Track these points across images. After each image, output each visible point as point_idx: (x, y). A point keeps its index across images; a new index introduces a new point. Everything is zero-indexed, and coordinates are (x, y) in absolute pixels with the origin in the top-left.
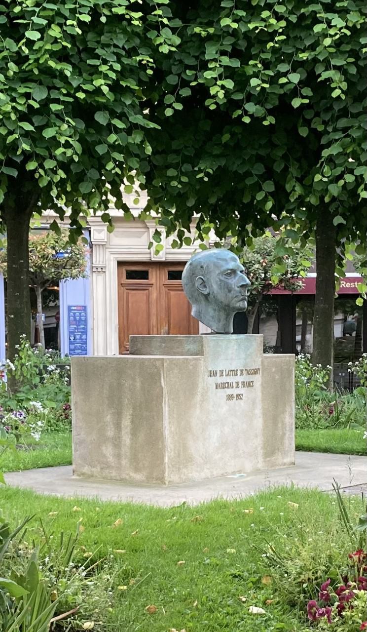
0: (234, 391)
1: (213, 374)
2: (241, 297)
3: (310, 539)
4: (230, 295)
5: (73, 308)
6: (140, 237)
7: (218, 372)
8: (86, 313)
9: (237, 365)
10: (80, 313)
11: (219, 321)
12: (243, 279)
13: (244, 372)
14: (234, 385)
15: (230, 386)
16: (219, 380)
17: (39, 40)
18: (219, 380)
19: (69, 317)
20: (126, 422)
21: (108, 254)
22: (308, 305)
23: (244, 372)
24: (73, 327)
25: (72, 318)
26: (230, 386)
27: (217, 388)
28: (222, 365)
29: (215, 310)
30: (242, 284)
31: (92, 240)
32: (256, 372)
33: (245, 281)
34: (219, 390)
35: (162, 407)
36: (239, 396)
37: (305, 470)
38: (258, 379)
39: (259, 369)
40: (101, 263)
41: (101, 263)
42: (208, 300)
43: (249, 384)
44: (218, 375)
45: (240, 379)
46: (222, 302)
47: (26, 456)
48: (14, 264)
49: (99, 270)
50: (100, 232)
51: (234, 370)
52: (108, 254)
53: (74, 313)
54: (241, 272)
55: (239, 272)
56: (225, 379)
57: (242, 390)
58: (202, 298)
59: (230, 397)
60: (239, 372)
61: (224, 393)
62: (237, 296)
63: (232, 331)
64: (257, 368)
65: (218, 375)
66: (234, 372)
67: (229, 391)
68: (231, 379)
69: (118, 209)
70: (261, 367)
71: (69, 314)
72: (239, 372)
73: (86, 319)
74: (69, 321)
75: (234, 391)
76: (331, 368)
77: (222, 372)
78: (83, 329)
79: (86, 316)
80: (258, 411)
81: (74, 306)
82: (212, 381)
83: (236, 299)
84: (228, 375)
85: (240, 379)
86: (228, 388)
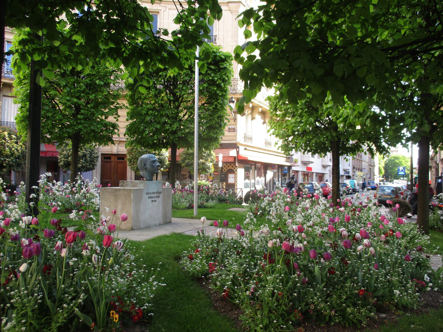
0: (154, 199)
1: (147, 194)
3: (64, 253)
9: (155, 190)
17: (358, 233)
22: (172, 246)
32: (160, 193)
36: (155, 201)
37: (205, 210)
45: (156, 195)
47: (288, 174)
57: (156, 199)
59: (152, 201)
61: (150, 200)
66: (154, 193)
67: (152, 199)
69: (145, 7)
75: (154, 199)
76: (235, 267)
80: (161, 205)
82: (147, 196)
85: (156, 195)
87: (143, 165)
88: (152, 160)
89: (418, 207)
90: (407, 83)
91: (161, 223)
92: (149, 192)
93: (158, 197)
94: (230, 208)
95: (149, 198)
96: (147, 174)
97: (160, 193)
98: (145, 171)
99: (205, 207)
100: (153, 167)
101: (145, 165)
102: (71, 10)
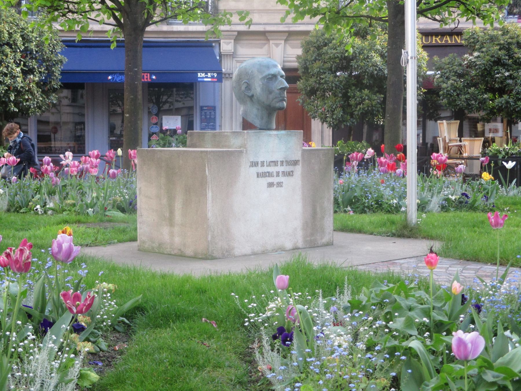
0: (275, 180)
1: (254, 164)
2: (281, 98)
4: (271, 97)
5: (205, 108)
6: (261, 48)
7: (260, 163)
8: (215, 113)
9: (278, 156)
10: (210, 113)
11: (262, 118)
12: (282, 83)
13: (284, 164)
14: (275, 174)
15: (269, 174)
16: (261, 170)
18: (261, 170)
19: (201, 116)
20: (178, 205)
21: (234, 62)
23: (284, 164)
24: (204, 124)
25: (203, 117)
26: (269, 174)
27: (258, 177)
28: (264, 156)
29: (258, 109)
30: (281, 87)
31: (221, 51)
32: (295, 163)
33: (284, 84)
34: (260, 179)
35: (206, 192)
36: (280, 184)
38: (298, 170)
39: (298, 161)
40: (228, 70)
41: (228, 70)
42: (252, 101)
43: (289, 174)
44: (260, 165)
45: (281, 169)
46: (263, 103)
48: (130, 71)
49: (227, 76)
50: (228, 44)
51: (274, 162)
52: (234, 62)
53: (205, 113)
54: (282, 76)
55: (279, 77)
56: (266, 169)
58: (248, 99)
59: (271, 185)
60: (279, 163)
62: (276, 98)
63: (274, 127)
64: (297, 159)
65: (260, 165)
67: (270, 180)
68: (273, 169)
70: (300, 159)
71: (201, 113)
72: (279, 163)
73: (215, 117)
74: (201, 119)
77: (263, 163)
78: (213, 126)
79: (215, 115)
81: (206, 107)
82: (254, 170)
83: (276, 100)
84: (269, 165)
85: (281, 169)
86: (269, 176)
87: (243, 88)
88: (267, 73)
89: (112, 224)
90: (397, 334)
91: (300, 244)
92: (260, 160)
93: (290, 174)
94: (208, 168)
95: (258, 175)
96: (255, 111)
97: (295, 163)
98: (249, 103)
99: (473, 208)
100: (270, 92)
101: (249, 87)
102: (515, 181)
